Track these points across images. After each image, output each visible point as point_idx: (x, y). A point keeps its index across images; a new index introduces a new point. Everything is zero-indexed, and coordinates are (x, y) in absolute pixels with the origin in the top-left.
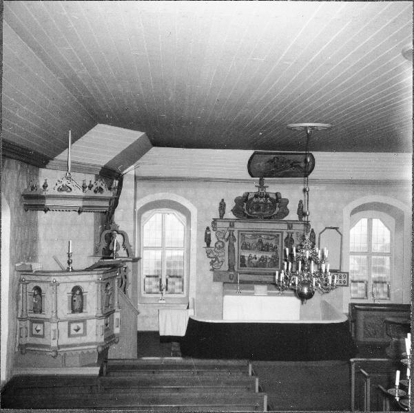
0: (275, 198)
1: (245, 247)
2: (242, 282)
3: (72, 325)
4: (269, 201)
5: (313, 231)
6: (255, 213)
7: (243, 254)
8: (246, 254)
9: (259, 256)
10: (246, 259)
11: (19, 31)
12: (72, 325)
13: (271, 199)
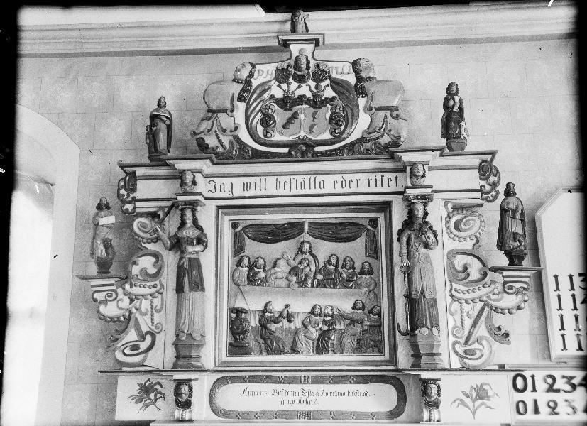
0: (352, 80)
1: (254, 276)
4: (329, 93)
5: (509, 192)
7: (240, 304)
8: (253, 302)
13: (336, 84)
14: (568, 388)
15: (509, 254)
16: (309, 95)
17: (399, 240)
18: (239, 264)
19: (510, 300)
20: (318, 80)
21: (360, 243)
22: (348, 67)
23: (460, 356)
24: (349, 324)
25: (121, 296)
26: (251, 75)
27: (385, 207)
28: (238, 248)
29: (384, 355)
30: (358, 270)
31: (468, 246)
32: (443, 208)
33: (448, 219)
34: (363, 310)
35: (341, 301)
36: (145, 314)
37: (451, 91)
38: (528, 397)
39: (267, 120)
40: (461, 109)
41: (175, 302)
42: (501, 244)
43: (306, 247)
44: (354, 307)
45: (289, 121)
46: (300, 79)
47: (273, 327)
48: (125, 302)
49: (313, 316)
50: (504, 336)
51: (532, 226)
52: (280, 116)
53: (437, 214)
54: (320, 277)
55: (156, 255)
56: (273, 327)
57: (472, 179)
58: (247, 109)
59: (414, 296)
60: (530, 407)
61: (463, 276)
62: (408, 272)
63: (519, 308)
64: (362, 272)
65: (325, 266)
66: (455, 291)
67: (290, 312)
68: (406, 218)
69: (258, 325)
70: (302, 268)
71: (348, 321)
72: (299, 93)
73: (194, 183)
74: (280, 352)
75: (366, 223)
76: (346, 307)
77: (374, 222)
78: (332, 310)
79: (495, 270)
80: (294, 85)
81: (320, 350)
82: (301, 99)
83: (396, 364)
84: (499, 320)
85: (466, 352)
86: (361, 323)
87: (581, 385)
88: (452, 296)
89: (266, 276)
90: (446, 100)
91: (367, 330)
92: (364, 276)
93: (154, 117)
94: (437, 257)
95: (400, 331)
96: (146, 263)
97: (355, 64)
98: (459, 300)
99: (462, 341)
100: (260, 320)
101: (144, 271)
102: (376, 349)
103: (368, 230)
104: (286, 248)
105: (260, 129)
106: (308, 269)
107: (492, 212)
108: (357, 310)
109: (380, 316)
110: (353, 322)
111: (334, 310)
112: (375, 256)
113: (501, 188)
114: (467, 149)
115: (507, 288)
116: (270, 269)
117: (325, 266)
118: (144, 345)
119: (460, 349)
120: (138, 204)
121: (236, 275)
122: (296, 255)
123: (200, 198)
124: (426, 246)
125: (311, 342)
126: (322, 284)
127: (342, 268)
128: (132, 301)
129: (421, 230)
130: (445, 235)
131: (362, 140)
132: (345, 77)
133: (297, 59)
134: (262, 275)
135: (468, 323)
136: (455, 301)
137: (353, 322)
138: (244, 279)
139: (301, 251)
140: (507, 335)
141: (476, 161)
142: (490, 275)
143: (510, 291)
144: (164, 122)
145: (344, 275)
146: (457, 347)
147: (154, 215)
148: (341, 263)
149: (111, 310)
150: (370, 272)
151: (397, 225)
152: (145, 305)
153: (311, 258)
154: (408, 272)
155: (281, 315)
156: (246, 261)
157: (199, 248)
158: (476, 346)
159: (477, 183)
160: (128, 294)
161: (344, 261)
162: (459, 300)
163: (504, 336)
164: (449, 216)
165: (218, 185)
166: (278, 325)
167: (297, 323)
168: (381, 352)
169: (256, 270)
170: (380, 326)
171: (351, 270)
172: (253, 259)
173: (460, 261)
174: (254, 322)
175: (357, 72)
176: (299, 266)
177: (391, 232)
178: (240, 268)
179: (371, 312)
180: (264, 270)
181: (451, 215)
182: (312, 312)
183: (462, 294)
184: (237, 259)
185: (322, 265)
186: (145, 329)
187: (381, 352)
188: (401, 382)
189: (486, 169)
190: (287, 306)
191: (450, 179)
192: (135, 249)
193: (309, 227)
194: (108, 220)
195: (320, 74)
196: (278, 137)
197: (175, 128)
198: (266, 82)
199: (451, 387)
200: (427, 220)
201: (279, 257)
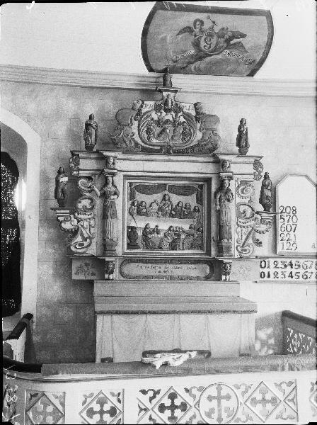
0: (193, 113)
1: (139, 210)
2: (177, 358)
3: (264, 18)
4: (182, 119)
5: (266, 177)
6: (154, 141)
7: (133, 224)
8: (140, 223)
9: (164, 226)
10: (140, 233)
11: (138, 422)
12: (264, 18)
13: (187, 116)
14: (283, 267)
15: (264, 206)
16: (171, 119)
17: (215, 197)
18: (133, 204)
19: (263, 227)
20: (176, 113)
22: (192, 106)
25: (73, 219)
26: (142, 106)
27: (208, 181)
28: (132, 196)
30: (192, 210)
31: (246, 201)
35: (184, 225)
36: (86, 228)
37: (242, 122)
38: (266, 271)
39: (149, 131)
40: (247, 133)
42: (261, 201)
45: (161, 133)
46: (167, 111)
47: (150, 236)
48: (75, 222)
50: (259, 243)
51: (274, 191)
52: (157, 130)
53: (233, 186)
54: (173, 212)
55: (91, 199)
56: (150, 236)
57: (250, 169)
58: (139, 125)
60: (266, 275)
61: (243, 215)
63: (267, 231)
72: (167, 118)
73: (114, 163)
74: (152, 248)
76: (186, 227)
77: (201, 187)
79: (258, 213)
80: (164, 113)
81: (173, 247)
82: (167, 121)
83: (210, 255)
84: (258, 236)
88: (238, 225)
90: (240, 128)
93: (88, 125)
96: (85, 203)
97: (195, 105)
101: (85, 207)
104: (158, 197)
105: (146, 136)
107: (258, 185)
113: (263, 174)
114: (248, 154)
115: (262, 221)
118: (86, 244)
119: (239, 249)
120: (80, 172)
123: (116, 171)
124: (229, 200)
126: (173, 216)
128: (79, 222)
129: (226, 193)
131: (197, 145)
132: (190, 112)
133: (167, 101)
134: (145, 211)
135: (244, 237)
140: (261, 243)
141: (252, 160)
142: (256, 216)
143: (240, 192)
144: (94, 128)
147: (89, 178)
149: (67, 226)
150: (199, 211)
151: (214, 189)
152: (86, 224)
154: (219, 212)
156: (136, 204)
157: (116, 196)
158: (247, 248)
159: (252, 171)
160: (77, 218)
163: (259, 243)
164: (238, 186)
165: (127, 165)
172: (140, 202)
174: (140, 233)
175: (196, 109)
177: (210, 193)
182: (170, 229)
186: (86, 236)
189: (257, 164)
190: (157, 226)
191: (239, 168)
192: (78, 195)
194: (64, 179)
195: (178, 109)
196: (154, 141)
197: (99, 131)
198: (149, 111)
199: (235, 268)
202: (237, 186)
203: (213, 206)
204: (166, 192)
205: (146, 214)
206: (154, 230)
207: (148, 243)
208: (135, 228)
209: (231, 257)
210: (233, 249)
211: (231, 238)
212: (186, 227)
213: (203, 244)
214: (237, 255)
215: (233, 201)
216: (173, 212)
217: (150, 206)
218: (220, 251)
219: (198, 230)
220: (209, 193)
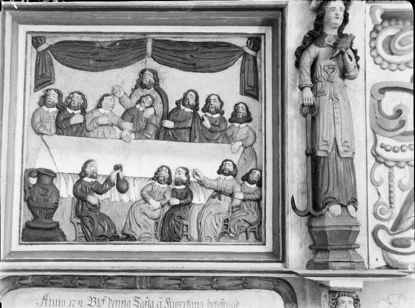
7: (42, 162)
8: (65, 159)
10: (66, 190)
17: (298, 64)
18: (44, 101)
21: (234, 71)
23: (384, 248)
24: (213, 197)
28: (43, 79)
29: (264, 244)
30: (227, 116)
32: (368, 16)
33: (374, 35)
34: (235, 176)
35: (202, 160)
41: (6, 155)
43: (149, 78)
44: (221, 171)
49: (157, 183)
56: (93, 199)
59: (320, 154)
62: (311, 113)
64: (234, 118)
65: (178, 108)
66: (382, 147)
67: (122, 177)
68: (312, 28)
69: (72, 196)
70: (141, 109)
71: (210, 192)
75: (241, 42)
76: (208, 170)
78: (187, 174)
83: (283, 260)
85: (393, 243)
86: (231, 195)
87: (411, 227)
88: (376, 156)
89: (85, 121)
91: (239, 206)
92: (237, 125)
94: (356, 93)
95: (294, 208)
98: (385, 162)
99: (389, 225)
100: (75, 187)
102: (252, 236)
103: (245, 54)
106: (151, 111)
108: (225, 174)
109: (259, 184)
110: (218, 193)
111: (190, 174)
112: (254, 93)
116: (91, 112)
117: (178, 108)
121: (37, 119)
122: (133, 90)
125: (153, 222)
127: (203, 110)
130: (370, 60)
136: (380, 163)
137: (218, 193)
138: (51, 126)
139: (141, 84)
145: (207, 123)
146: (381, 235)
148: (202, 104)
150: (248, 119)
151: (293, 39)
153: (156, 95)
154: (311, 113)
155: (108, 180)
161: (208, 101)
162: (385, 162)
164: (375, 30)
166: (104, 197)
167: (134, 193)
168: (260, 239)
169: (70, 111)
170: (258, 201)
171: (218, 115)
172: (65, 95)
173: (390, 102)
174: (66, 190)
176: (138, 106)
178: (45, 108)
179: (246, 178)
180: (84, 112)
181: (379, 28)
182: (156, 178)
183: (392, 152)
184: (41, 93)
185: (172, 106)
187: (260, 239)
188: (294, 293)
190: (118, 168)
193: (153, 46)
200: (344, 32)
201: (107, 92)
202: (370, 27)
203: (293, 95)
204: (151, 64)
205: (81, 130)
206: (108, 180)
207: (93, 225)
208: (52, 175)
209: (355, 269)
210: (361, 239)
211: (354, 202)
212: (208, 170)
213: (260, 223)
214: (375, 258)
215: (359, 80)
216: (169, 124)
217: (99, 106)
218: (320, 244)
219: (246, 178)
220: (337, 302)
